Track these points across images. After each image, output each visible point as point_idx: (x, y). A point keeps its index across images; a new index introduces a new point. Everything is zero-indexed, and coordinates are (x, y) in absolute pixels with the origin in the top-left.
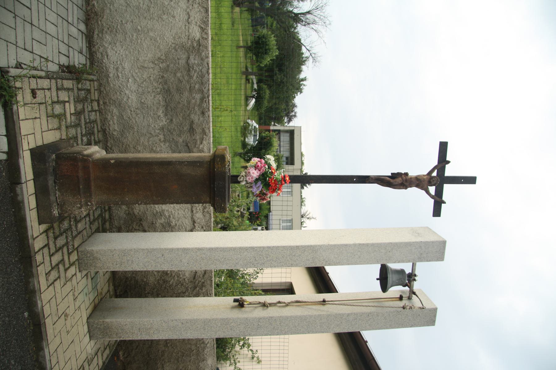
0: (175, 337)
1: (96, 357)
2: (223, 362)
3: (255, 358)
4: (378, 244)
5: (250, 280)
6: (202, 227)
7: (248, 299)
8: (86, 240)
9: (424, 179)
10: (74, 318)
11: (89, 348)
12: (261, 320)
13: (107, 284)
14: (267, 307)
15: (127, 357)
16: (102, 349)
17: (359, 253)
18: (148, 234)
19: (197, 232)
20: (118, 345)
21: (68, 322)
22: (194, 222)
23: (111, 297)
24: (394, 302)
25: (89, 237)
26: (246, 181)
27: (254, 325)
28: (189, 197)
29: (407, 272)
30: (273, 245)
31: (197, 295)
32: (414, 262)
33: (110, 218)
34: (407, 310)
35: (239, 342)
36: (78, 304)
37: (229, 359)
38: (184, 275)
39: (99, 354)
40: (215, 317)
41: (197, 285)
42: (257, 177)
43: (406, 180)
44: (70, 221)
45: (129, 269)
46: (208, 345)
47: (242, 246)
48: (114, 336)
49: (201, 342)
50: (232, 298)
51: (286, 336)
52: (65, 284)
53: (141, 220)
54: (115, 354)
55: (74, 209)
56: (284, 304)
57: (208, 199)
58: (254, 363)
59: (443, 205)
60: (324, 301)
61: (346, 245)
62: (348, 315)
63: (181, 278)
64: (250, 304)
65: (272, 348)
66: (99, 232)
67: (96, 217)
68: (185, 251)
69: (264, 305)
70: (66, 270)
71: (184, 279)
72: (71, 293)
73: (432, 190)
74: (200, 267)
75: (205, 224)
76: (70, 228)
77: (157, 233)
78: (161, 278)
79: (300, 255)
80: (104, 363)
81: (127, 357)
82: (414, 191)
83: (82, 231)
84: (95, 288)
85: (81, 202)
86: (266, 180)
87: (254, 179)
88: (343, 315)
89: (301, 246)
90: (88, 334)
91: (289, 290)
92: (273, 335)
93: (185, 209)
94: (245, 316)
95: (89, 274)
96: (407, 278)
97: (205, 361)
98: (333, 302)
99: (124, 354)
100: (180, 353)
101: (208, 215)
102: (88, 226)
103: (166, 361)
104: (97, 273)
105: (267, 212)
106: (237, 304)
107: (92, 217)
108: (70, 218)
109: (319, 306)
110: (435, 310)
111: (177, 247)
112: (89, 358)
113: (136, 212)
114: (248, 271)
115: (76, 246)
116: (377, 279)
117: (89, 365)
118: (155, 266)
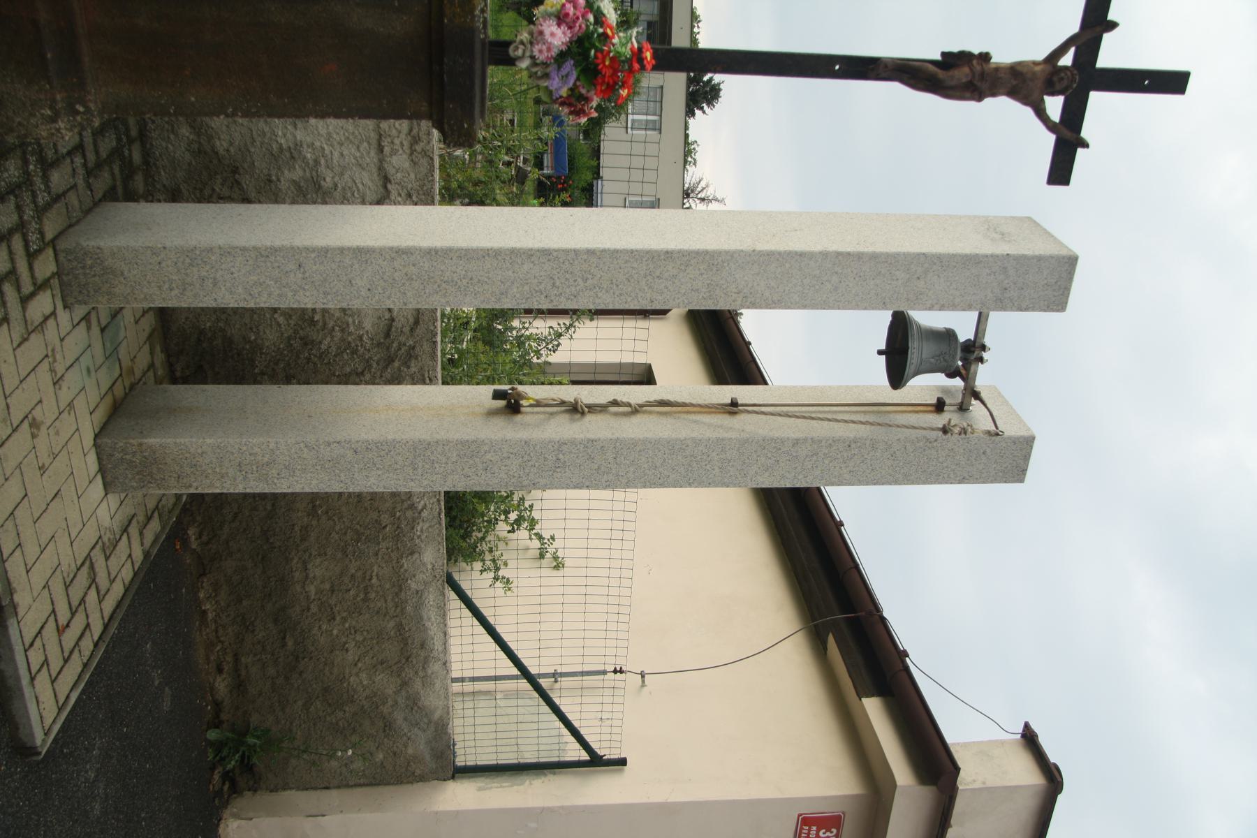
0: (337, 487)
1: (125, 537)
2: (464, 565)
3: (547, 556)
4: (888, 255)
5: (538, 353)
6: (409, 196)
7: (532, 392)
8: (78, 222)
9: (1034, 73)
10: (57, 433)
11: (104, 514)
12: (564, 448)
13: (147, 348)
14: (583, 413)
15: (207, 543)
16: (141, 518)
17: (835, 279)
18: (252, 206)
19: (393, 208)
20: (185, 510)
21: (42, 442)
22: (386, 180)
23: (159, 381)
24: (921, 416)
25: (88, 212)
26: (532, 57)
28: (369, 99)
29: (962, 339)
30: (601, 246)
31: (396, 380)
32: (984, 311)
33: (146, 162)
34: (954, 438)
35: (506, 513)
36: (65, 395)
37: (480, 556)
38: (360, 326)
39: (134, 530)
40: (443, 435)
41: (392, 351)
42: (564, 48)
43: (983, 75)
44: (26, 162)
45: (208, 302)
46: (425, 514)
47: (518, 245)
48: (173, 482)
49: (406, 505)
50: (487, 390)
51: (631, 494)
52: (25, 340)
53: (235, 170)
54: (175, 535)
55: (33, 121)
56: (629, 409)
57: (424, 107)
58: (546, 572)
59: (1080, 151)
60: (734, 404)
61: (801, 255)
62: (796, 442)
63: (350, 334)
64: (538, 404)
65: (592, 534)
66: (117, 200)
67: (104, 155)
68: (363, 254)
69: (575, 409)
70: (25, 301)
71: (361, 338)
72: (45, 366)
73: (1054, 106)
74: (404, 300)
75: (416, 185)
76: (27, 180)
77: (283, 206)
78: (296, 332)
79: (674, 276)
80: (147, 555)
81: (207, 543)
82: (1003, 112)
83: (64, 194)
84: (111, 354)
85: (54, 101)
86: (586, 56)
87: (554, 52)
88: (783, 441)
89: (679, 252)
90: (99, 477)
91: (646, 377)
92: (597, 487)
93: (361, 142)
94: (523, 435)
95: (93, 316)
96: (959, 354)
97: (416, 556)
98: (755, 408)
99: (200, 536)
100: (350, 534)
101: (424, 161)
102: (80, 181)
103: (314, 553)
104: (115, 314)
105: (588, 176)
106: (502, 403)
107: (91, 157)
108: (24, 153)
109: (720, 416)
110: (1029, 442)
111: (338, 243)
112: (105, 539)
113: (221, 145)
114: (535, 331)
115: (49, 236)
116: (880, 353)
117: (107, 558)
118: (280, 295)
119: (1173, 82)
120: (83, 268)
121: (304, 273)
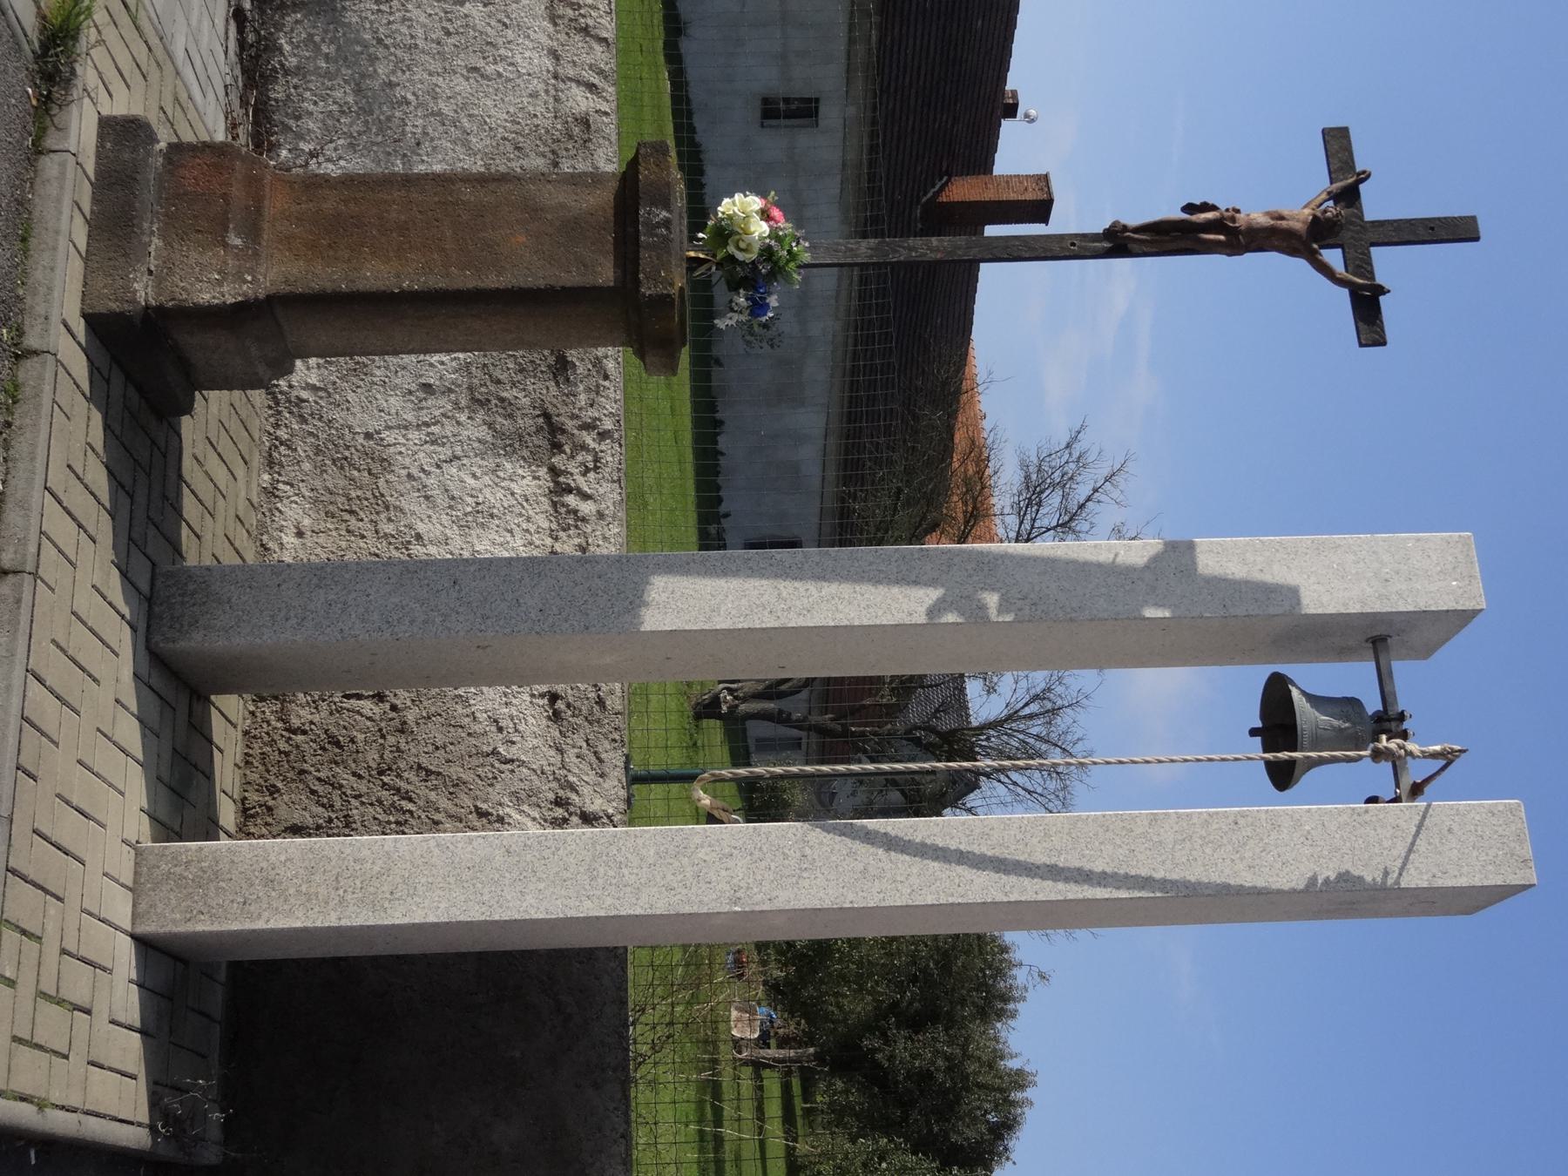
27: (786, 856)
59: (1381, 298)
116: (1254, 732)
119: (1460, 230)
120: (182, 595)
121: (460, 591)
